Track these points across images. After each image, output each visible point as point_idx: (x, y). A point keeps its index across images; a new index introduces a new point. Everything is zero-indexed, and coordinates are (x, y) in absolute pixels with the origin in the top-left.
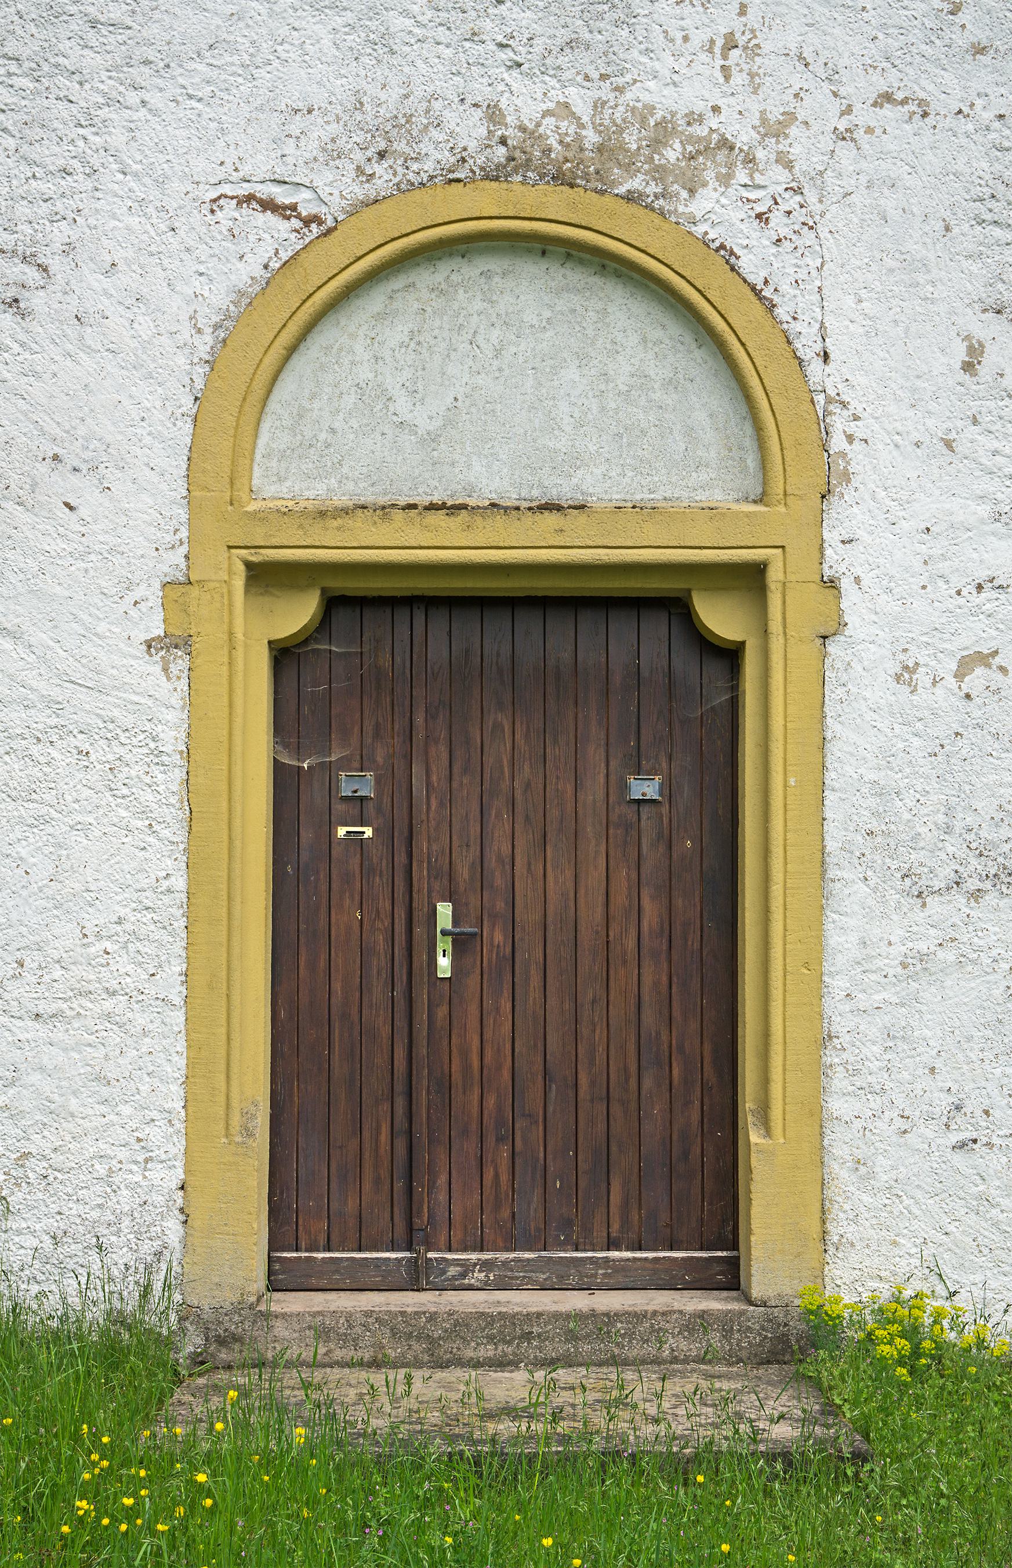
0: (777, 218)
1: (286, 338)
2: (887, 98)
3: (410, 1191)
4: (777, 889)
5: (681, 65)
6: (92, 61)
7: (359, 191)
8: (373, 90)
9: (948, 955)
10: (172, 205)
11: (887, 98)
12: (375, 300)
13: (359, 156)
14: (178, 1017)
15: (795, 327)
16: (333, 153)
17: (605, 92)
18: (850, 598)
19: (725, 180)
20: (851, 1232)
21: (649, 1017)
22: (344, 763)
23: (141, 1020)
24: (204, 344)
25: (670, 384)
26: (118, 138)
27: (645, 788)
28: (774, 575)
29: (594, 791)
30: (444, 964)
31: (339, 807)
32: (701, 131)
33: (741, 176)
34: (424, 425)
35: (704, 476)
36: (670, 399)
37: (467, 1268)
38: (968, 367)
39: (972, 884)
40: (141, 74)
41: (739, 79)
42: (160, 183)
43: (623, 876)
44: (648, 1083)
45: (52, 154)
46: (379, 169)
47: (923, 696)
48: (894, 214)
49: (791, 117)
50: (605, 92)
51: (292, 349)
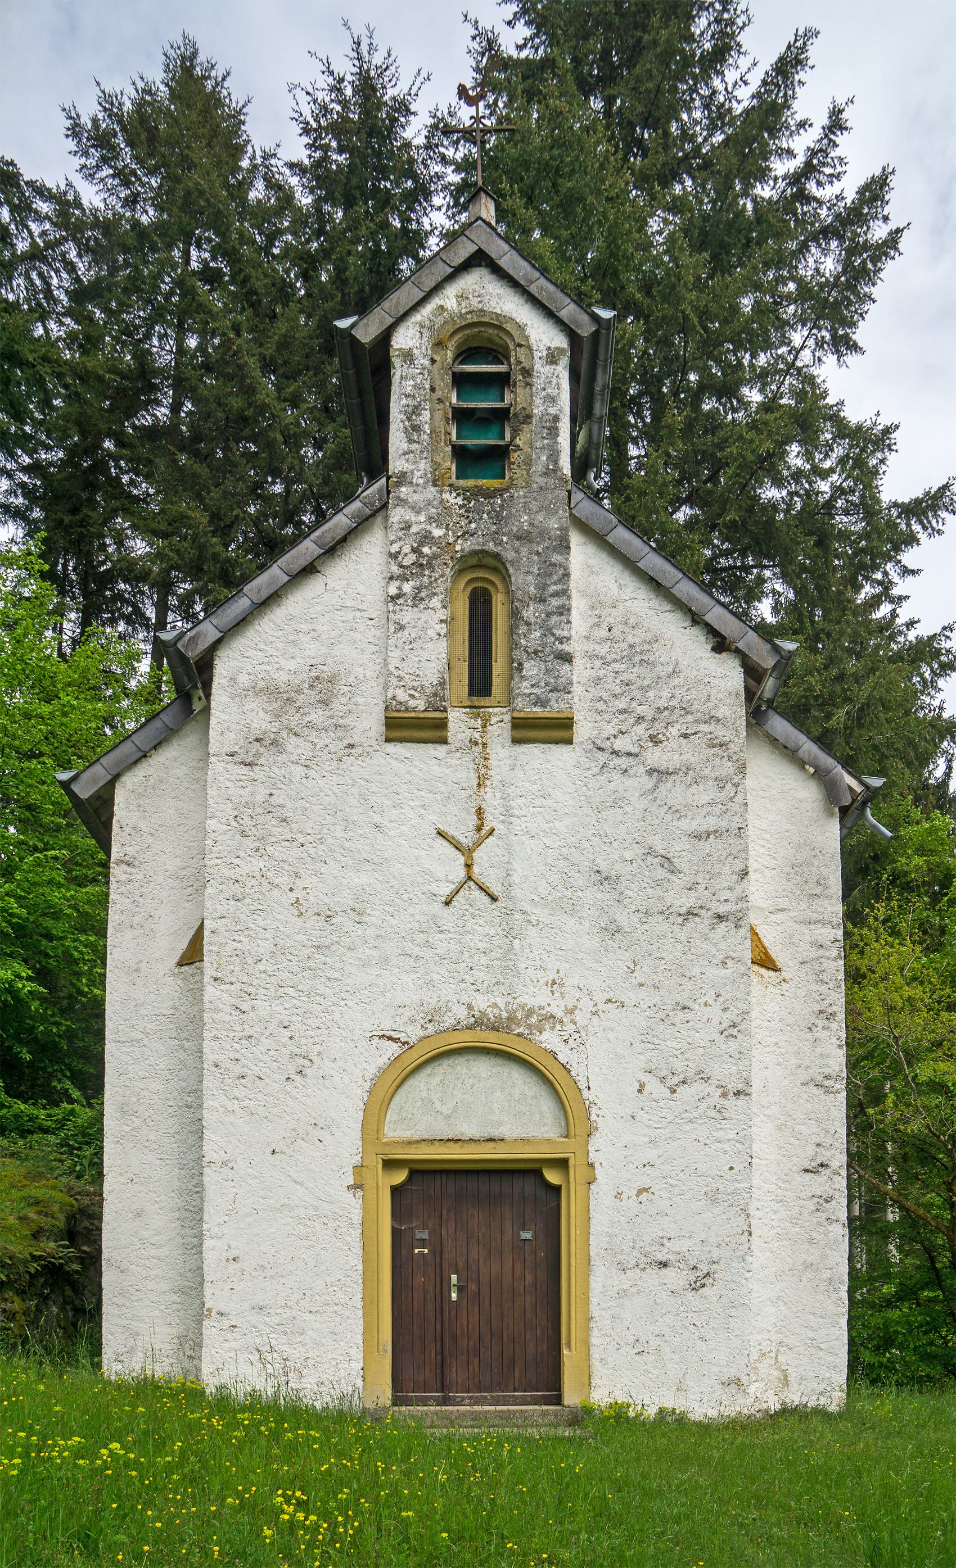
0: (571, 1041)
1: (396, 1083)
2: (610, 1001)
3: (442, 1373)
4: (573, 1269)
5: (536, 990)
6: (328, 991)
7: (422, 1033)
8: (427, 999)
9: (634, 1290)
10: (356, 1038)
11: (610, 1001)
12: (428, 1070)
13: (422, 1022)
14: (361, 1312)
15: (577, 1078)
16: (412, 1021)
17: (509, 999)
18: (599, 1171)
19: (553, 1028)
20: (599, 1382)
21: (528, 1314)
22: (418, 1227)
23: (347, 1314)
24: (367, 1086)
25: (534, 1097)
26: (337, 1016)
27: (527, 1235)
28: (571, 1162)
29: (508, 1236)
30: (454, 1296)
31: (416, 1243)
32: (544, 1012)
33: (558, 1027)
34: (446, 1112)
35: (546, 1129)
36: (534, 1103)
37: (463, 1399)
38: (640, 1091)
39: (642, 1266)
40: (344, 995)
41: (557, 994)
42: (352, 1031)
43: (519, 1266)
44: (528, 1336)
45: (313, 1022)
46: (429, 1026)
47: (625, 1202)
48: (613, 1040)
49: (575, 1007)
50: (509, 999)
51: (398, 1087)
